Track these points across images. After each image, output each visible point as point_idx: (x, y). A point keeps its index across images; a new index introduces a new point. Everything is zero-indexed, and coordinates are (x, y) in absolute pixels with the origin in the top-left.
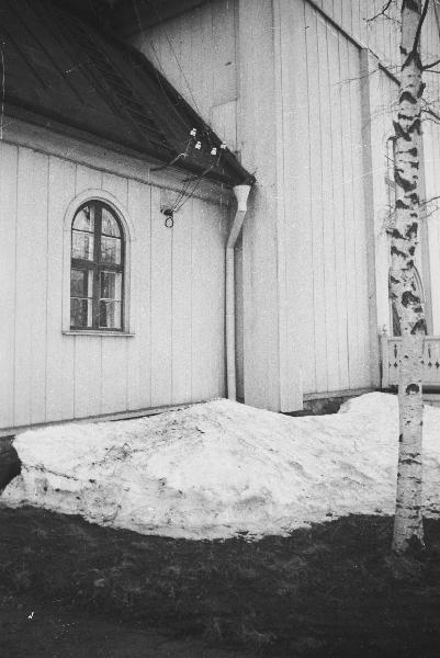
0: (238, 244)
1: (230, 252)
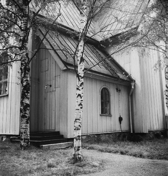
0: (132, 96)
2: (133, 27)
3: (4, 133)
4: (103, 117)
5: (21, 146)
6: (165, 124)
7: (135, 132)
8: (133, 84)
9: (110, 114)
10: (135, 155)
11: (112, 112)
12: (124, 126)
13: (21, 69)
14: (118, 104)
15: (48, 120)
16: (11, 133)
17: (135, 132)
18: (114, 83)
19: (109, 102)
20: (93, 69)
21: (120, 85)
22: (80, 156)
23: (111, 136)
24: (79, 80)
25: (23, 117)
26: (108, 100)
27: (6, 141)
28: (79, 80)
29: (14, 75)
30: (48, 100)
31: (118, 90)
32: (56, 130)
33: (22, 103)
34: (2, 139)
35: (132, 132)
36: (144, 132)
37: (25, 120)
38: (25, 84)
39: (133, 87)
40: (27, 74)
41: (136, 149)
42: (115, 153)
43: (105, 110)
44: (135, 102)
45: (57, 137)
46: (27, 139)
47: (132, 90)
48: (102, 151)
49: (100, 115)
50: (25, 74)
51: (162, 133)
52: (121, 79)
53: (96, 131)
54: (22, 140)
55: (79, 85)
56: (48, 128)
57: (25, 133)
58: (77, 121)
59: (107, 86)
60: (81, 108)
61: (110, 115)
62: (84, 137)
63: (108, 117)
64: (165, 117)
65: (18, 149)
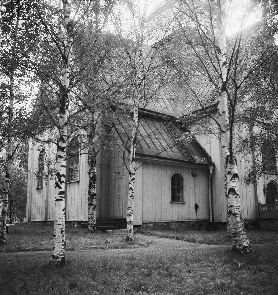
0: (211, 181)
1: (210, 182)
2: (213, 103)
3: (75, 220)
4: (174, 205)
5: (89, 230)
6: (258, 213)
7: (215, 221)
8: (211, 168)
9: (183, 201)
10: (188, 241)
11: (186, 200)
12: (202, 215)
13: (89, 162)
14: (194, 191)
15: (117, 206)
16: (82, 220)
17: (215, 221)
18: (188, 168)
19: (182, 188)
20: (162, 155)
21: (196, 169)
22: (131, 237)
23: (183, 224)
24: (131, 176)
25: (90, 204)
26: (181, 186)
27: (76, 227)
28: (131, 176)
29: (84, 163)
30: (117, 187)
31: (194, 175)
32: (124, 218)
33: (89, 192)
34: (74, 226)
35: (211, 221)
36: (223, 221)
37: (92, 207)
38: (92, 175)
39: (211, 171)
40: (94, 166)
41: (209, 236)
42: (172, 238)
43: (177, 196)
44: (215, 187)
45: (122, 223)
46: (94, 224)
47: (211, 175)
48: (161, 237)
49: (171, 202)
50: (92, 167)
51: (252, 223)
52: (199, 164)
53: (164, 219)
54: (89, 224)
55: (130, 180)
56: (117, 216)
57: (92, 218)
58: (129, 209)
59: (180, 171)
60: (132, 199)
61: (183, 203)
62: (151, 224)
63: (180, 205)
64: (257, 204)
65: (86, 233)
